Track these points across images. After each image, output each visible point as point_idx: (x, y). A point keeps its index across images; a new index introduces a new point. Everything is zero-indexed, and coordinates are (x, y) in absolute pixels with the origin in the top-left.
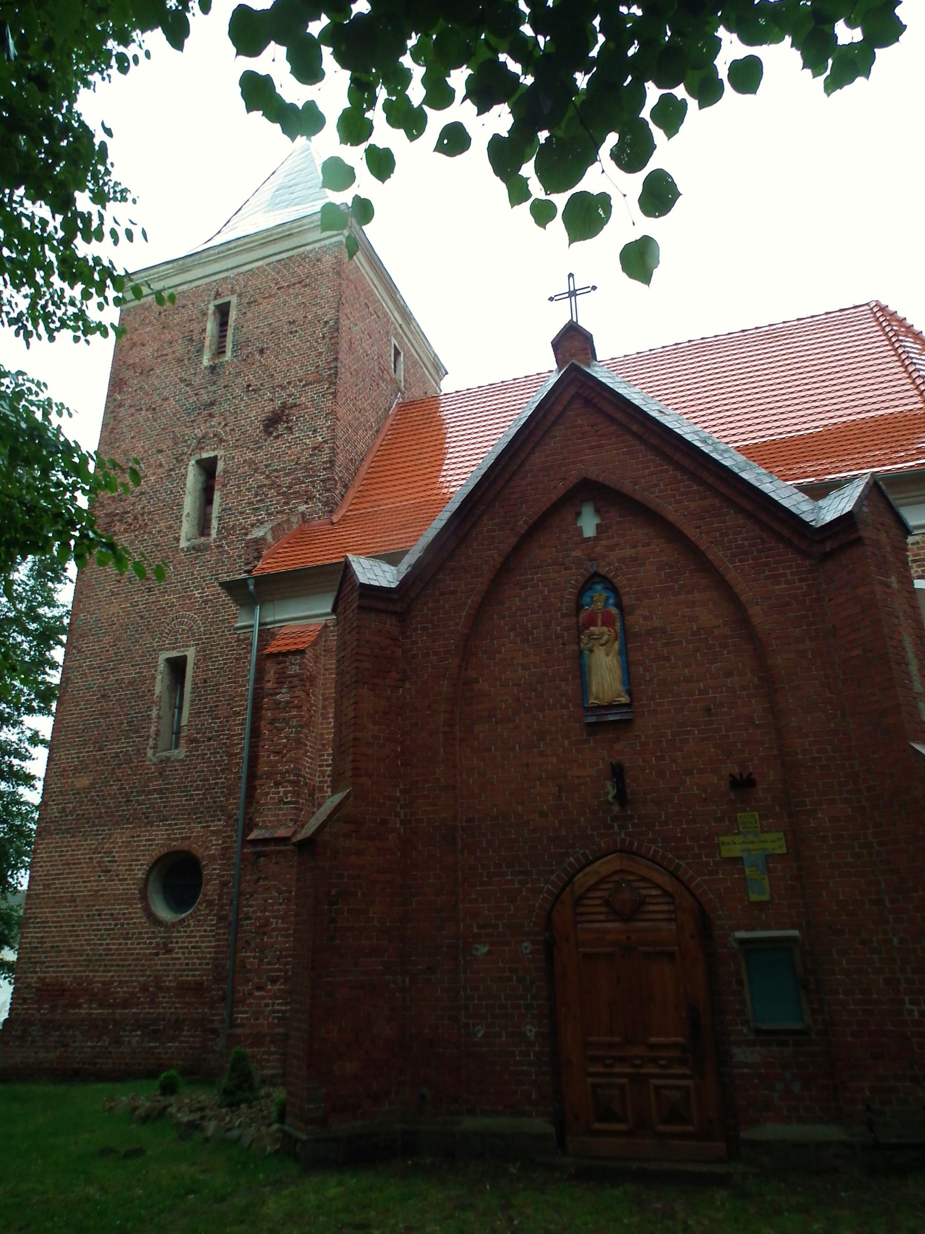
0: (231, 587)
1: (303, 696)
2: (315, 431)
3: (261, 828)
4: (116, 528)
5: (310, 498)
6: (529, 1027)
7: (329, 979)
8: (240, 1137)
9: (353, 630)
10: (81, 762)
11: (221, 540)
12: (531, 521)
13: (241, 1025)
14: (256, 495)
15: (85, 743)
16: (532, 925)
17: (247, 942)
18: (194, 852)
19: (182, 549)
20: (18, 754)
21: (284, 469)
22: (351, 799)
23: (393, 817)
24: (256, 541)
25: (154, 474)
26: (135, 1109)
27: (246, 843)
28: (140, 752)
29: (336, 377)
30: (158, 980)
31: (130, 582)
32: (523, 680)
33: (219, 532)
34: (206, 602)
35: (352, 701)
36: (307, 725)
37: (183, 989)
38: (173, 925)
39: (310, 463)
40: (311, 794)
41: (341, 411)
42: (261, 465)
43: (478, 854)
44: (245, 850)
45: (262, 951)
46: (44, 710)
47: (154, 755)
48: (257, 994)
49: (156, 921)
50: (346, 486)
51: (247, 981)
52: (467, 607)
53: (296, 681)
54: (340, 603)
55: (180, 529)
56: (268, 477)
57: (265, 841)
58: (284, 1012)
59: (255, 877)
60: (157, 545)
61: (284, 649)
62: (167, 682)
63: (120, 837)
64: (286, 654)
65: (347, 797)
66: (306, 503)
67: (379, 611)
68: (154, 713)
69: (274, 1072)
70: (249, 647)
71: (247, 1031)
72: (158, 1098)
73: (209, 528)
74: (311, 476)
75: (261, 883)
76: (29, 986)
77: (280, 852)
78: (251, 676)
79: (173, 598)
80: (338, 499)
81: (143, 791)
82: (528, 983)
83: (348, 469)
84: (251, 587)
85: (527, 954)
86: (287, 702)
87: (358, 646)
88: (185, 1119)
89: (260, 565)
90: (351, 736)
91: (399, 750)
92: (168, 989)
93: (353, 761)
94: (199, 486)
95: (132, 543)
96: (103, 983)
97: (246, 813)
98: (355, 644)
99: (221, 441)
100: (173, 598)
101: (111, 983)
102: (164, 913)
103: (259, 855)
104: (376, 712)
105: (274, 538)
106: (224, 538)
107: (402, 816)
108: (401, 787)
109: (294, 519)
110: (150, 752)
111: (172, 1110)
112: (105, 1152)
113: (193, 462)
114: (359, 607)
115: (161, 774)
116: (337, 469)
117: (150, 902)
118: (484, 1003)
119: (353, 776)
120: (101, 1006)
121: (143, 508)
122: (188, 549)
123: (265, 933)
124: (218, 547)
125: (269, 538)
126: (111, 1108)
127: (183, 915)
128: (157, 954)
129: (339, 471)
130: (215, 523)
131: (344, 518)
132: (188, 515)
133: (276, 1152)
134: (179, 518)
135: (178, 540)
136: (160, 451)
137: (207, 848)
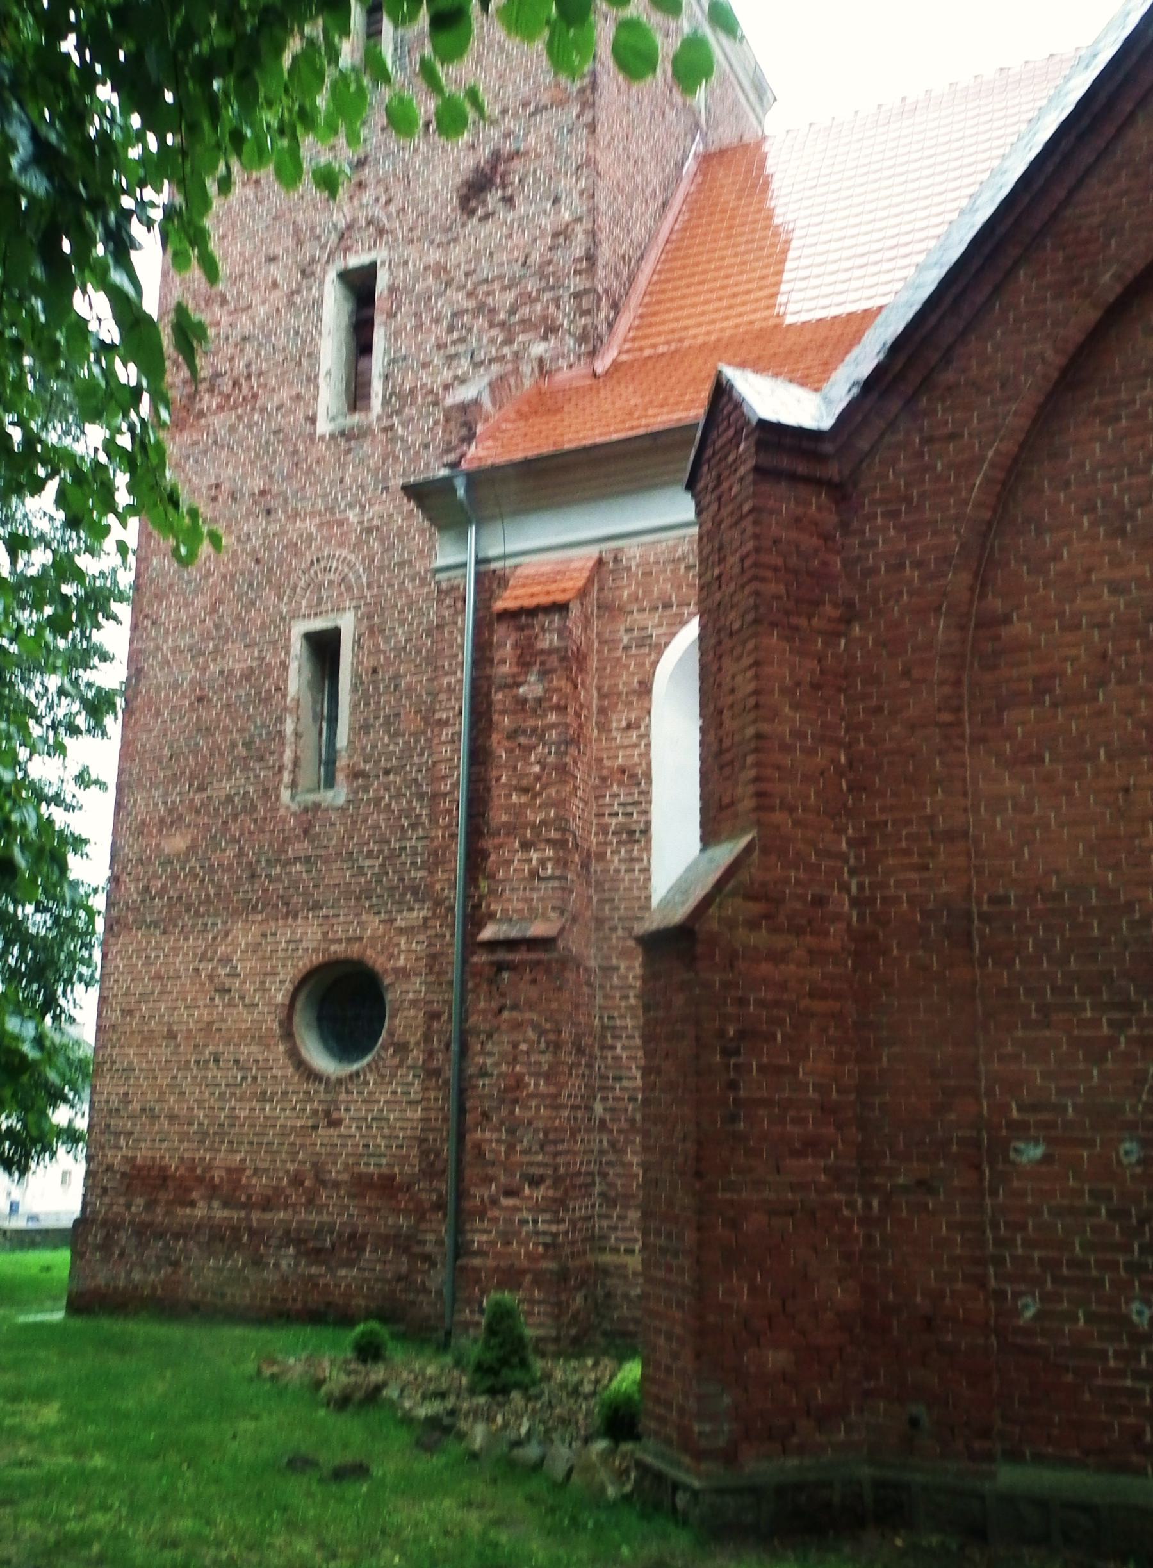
0: (417, 492)
1: (568, 688)
2: (556, 201)
3: (500, 921)
4: (204, 405)
5: (551, 330)
6: (1136, 1306)
7: (728, 1196)
8: (542, 1459)
9: (742, 517)
10: (170, 812)
11: (390, 416)
12: (1130, 275)
13: (481, 1253)
14: (451, 329)
15: (174, 779)
16: (1140, 1108)
17: (486, 1116)
18: (370, 963)
19: (322, 438)
20: (57, 800)
21: (501, 277)
22: (756, 853)
23: (836, 892)
24: (464, 408)
25: (264, 302)
26: (318, 1384)
27: (470, 944)
28: (268, 794)
29: (593, 92)
30: (318, 1170)
31: (234, 499)
32: (1112, 616)
33: (386, 402)
34: (369, 531)
35: (747, 661)
36: (575, 741)
37: (362, 1185)
38: (340, 1081)
39: (550, 262)
40: (585, 865)
41: (605, 161)
42: (459, 276)
43: (1018, 966)
44: (475, 959)
45: (511, 1131)
46: (98, 728)
47: (293, 797)
48: (507, 1202)
49: (311, 1075)
50: (615, 306)
51: (488, 1180)
52: (986, 466)
53: (553, 662)
54: (705, 468)
55: (315, 398)
56: (470, 295)
57: (510, 944)
58: (555, 1235)
59: (494, 1005)
60: (276, 433)
61: (528, 603)
62: (307, 673)
63: (244, 934)
64: (532, 612)
65: (748, 849)
66: (545, 338)
67: (793, 478)
68: (289, 727)
69: (541, 1332)
70: (459, 604)
71: (491, 1263)
72: (353, 1366)
73: (368, 397)
74: (552, 288)
75: (506, 1014)
76: (110, 1168)
77: (538, 963)
78: (467, 656)
79: (310, 525)
80: (603, 329)
81: (278, 860)
82: (1134, 1221)
83: (617, 275)
84: (461, 492)
85: (1130, 1164)
86: (539, 701)
87: (757, 550)
88: (422, 1412)
89: (472, 451)
90: (750, 731)
91: (843, 759)
92: (336, 1185)
93: (757, 779)
94: (345, 320)
95: (232, 429)
96: (229, 1170)
97: (467, 897)
98: (750, 545)
99: (381, 232)
100: (310, 525)
101: (241, 1170)
102: (321, 1061)
103: (500, 967)
104: (798, 684)
105: (494, 403)
106: (398, 412)
107: (854, 889)
108: (850, 831)
109: (526, 369)
110: (285, 794)
111: (391, 1392)
112: (299, 1464)
113: (332, 275)
114: (757, 469)
115: (306, 832)
116: (600, 273)
117: (298, 1042)
118: (1036, 1254)
119: (759, 808)
120: (226, 1205)
121: (248, 365)
122: (332, 436)
123: (516, 1101)
124: (385, 430)
125: (486, 401)
126: (273, 1377)
127: (355, 1067)
128: (315, 1128)
129: (604, 278)
130: (377, 387)
131: (616, 366)
132: (329, 373)
133: (626, 1498)
134: (312, 380)
135: (312, 420)
136: (272, 259)
137: (391, 956)
